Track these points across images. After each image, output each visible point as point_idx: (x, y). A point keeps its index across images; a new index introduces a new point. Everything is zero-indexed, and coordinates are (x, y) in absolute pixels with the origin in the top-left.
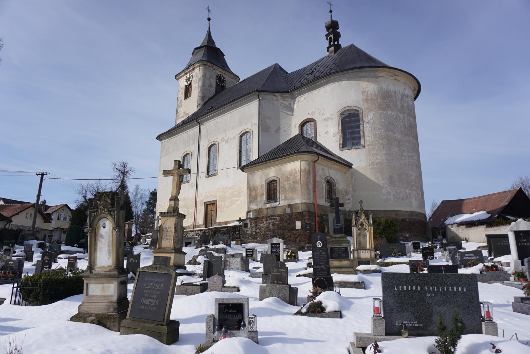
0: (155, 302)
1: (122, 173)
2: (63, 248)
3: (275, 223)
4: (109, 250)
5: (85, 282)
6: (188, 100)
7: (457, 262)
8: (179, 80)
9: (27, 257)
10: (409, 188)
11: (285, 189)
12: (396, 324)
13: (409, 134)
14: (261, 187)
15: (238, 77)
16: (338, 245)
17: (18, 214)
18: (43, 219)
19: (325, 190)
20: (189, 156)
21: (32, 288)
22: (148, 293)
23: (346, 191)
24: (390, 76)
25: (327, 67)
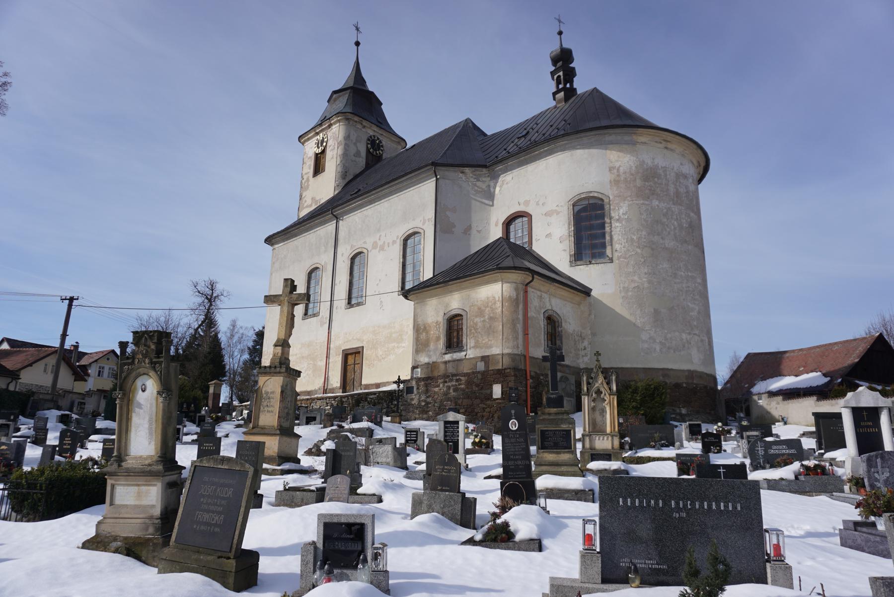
0: (218, 519)
1: (207, 298)
2: (100, 424)
3: (459, 387)
4: (150, 429)
5: (109, 482)
6: (320, 177)
7: (759, 459)
8: (305, 145)
9: (36, 438)
10: (688, 331)
11: (476, 329)
12: (621, 564)
13: (687, 240)
14: (437, 325)
15: (404, 140)
16: (554, 426)
17: (31, 366)
18: (73, 374)
19: (544, 332)
20: (319, 272)
21: (27, 490)
23: (581, 335)
25: (551, 126)
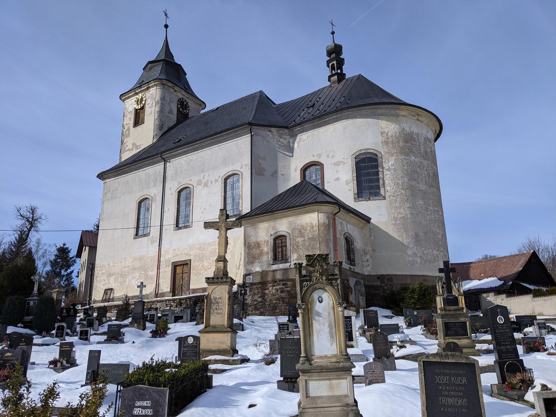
1: (28, 221)
6: (139, 128)
8: (125, 102)
15: (205, 103)
16: (455, 319)
22: (446, 390)
24: (412, 115)
25: (334, 100)
